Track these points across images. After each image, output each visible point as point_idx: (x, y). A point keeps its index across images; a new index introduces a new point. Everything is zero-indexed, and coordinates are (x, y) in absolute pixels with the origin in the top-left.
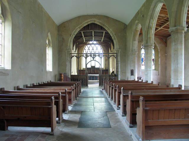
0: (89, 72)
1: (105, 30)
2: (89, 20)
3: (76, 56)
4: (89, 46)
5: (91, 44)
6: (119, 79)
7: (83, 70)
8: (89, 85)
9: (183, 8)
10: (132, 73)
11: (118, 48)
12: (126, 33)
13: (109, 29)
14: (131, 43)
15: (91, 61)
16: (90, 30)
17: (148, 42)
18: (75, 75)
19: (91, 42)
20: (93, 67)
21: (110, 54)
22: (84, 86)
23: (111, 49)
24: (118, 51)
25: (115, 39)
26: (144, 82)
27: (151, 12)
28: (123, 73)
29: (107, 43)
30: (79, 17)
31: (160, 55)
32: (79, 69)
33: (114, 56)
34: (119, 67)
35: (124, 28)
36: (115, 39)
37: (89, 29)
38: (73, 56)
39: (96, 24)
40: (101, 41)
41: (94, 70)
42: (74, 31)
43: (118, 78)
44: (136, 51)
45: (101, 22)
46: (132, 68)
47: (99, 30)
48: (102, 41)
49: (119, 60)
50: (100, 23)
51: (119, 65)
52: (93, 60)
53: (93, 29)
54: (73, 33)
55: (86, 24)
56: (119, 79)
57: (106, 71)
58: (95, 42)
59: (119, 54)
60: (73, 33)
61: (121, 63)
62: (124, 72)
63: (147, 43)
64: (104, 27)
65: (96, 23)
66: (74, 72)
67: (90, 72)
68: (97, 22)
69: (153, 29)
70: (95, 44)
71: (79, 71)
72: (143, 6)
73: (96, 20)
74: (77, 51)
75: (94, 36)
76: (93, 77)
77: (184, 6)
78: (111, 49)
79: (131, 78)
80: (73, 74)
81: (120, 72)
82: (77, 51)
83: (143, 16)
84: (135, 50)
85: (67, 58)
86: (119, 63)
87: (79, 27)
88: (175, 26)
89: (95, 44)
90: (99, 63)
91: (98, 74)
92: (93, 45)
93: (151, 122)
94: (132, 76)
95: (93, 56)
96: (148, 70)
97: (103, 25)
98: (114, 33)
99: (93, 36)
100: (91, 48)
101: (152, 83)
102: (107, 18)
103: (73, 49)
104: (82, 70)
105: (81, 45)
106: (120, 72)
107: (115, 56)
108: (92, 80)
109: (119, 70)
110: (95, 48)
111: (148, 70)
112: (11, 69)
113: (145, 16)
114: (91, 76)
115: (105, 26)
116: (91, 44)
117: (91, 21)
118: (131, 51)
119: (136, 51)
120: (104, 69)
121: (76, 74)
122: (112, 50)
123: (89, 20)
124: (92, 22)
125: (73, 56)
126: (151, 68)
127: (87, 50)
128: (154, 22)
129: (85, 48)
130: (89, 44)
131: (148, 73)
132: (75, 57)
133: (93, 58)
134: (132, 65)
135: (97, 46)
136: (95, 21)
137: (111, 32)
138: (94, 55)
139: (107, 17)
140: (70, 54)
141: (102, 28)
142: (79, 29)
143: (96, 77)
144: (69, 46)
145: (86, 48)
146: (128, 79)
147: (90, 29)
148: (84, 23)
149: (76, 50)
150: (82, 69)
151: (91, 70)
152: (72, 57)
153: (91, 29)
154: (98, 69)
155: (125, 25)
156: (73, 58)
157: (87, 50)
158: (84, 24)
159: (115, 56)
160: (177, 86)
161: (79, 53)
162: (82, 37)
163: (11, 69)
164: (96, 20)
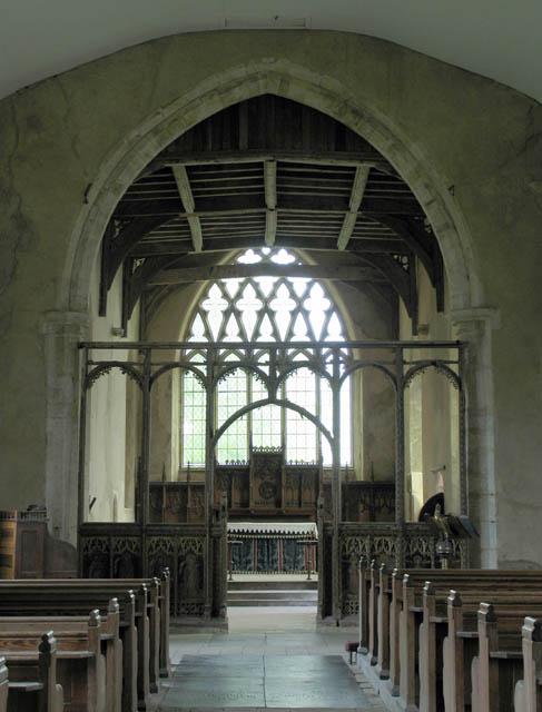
0: (236, 498)
1: (365, 150)
2: (240, 72)
3: (125, 367)
4: (232, 284)
6: (491, 563)
7: (187, 489)
8: (231, 612)
11: (477, 300)
13: (399, 145)
15: (247, 410)
18: (114, 529)
19: (249, 257)
21: (367, 541)
22: (194, 620)
23: (413, 313)
24: (479, 324)
30: (152, 42)
32: (153, 477)
34: (489, 462)
36: (450, 226)
38: (105, 367)
40: (332, 243)
41: (276, 489)
42: (119, 154)
45: (332, 84)
48: (342, 244)
49: (486, 398)
50: (329, 95)
51: (489, 441)
52: (272, 400)
54: (104, 175)
56: (491, 563)
57: (375, 492)
58: (284, 257)
59: (486, 356)
60: (104, 175)
65: (293, 93)
66: (111, 499)
67: (245, 503)
68: (306, 87)
70: (283, 272)
71: (151, 490)
73: (295, 70)
74: (132, 324)
75: (281, 202)
76: (267, 542)
78: (413, 313)
80: (99, 514)
81: (492, 500)
82: (132, 324)
85: (51, 380)
86: (488, 423)
87: (155, 131)
90: (315, 426)
91: (304, 518)
92: (266, 282)
97: (355, 112)
99: (271, 200)
100: (249, 305)
102: (384, 54)
103: (102, 311)
104: (173, 488)
106: (492, 500)
107: (455, 368)
109: (491, 484)
110: (283, 305)
114: (246, 539)
115: (371, 120)
116: (248, 272)
117: (253, 78)
120: (361, 477)
121: (125, 516)
122: (422, 320)
123: (240, 72)
125: (105, 367)
127: (215, 323)
129: (205, 305)
132: (116, 371)
133: (273, 383)
135: (300, 284)
136: (285, 79)
140: (81, 346)
141: (342, 138)
142: (154, 140)
143: (292, 541)
144: (73, 284)
147: (243, 143)
149: (125, 316)
150: (173, 476)
151: (245, 487)
152: (95, 375)
153: (253, 148)
154: (310, 476)
156: (101, 383)
157: (215, 323)
159: (455, 368)
161: (155, 337)
164: (295, 70)
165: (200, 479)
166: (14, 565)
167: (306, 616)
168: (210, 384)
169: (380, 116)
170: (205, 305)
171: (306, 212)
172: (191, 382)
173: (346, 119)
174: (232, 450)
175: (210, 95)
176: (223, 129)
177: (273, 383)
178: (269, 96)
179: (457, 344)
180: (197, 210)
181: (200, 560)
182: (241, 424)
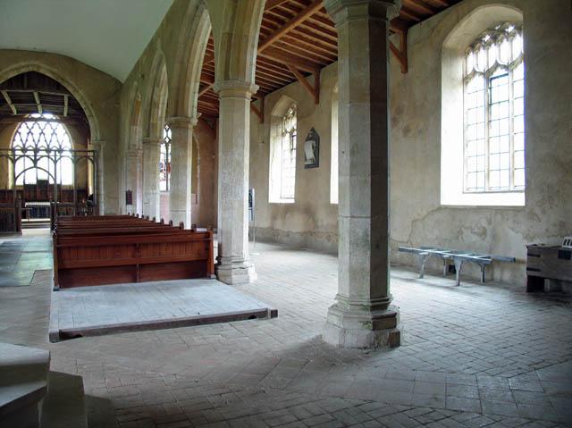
1: (68, 92)
2: (23, 64)
4: (30, 124)
5: (33, 119)
6: (102, 214)
8: (23, 230)
9: (187, 84)
10: (130, 199)
12: (118, 103)
13: (75, 90)
14: (127, 130)
15: (24, 171)
16: (27, 89)
17: (151, 135)
19: (35, 116)
20: (42, 184)
24: (100, 146)
25: (91, 116)
26: (102, 218)
27: (155, 72)
28: (110, 198)
29: (77, 122)
31: (199, 158)
33: (48, 157)
34: (102, 186)
35: (112, 91)
36: (91, 116)
37: (22, 85)
39: (44, 76)
40: (62, 114)
41: (46, 192)
43: (97, 207)
44: (137, 147)
45: (55, 70)
46: (129, 188)
47: (50, 90)
48: (65, 114)
49: (101, 166)
50: (53, 73)
51: (102, 179)
53: (34, 88)
55: (15, 74)
56: (102, 214)
58: (48, 116)
59: (102, 155)
61: (106, 174)
62: (112, 196)
63: (148, 136)
64: (65, 85)
65: (42, 71)
66: (10, 187)
67: (36, 196)
68: (45, 70)
69: (160, 106)
70: (49, 121)
72: (144, 54)
73: (42, 65)
77: (189, 81)
79: (126, 210)
83: (143, 76)
84: (134, 145)
86: (102, 174)
88: (176, 116)
89: (49, 121)
91: (48, 201)
92: (42, 124)
93: (68, 264)
94: (129, 206)
95: (53, 158)
96: (149, 194)
97: (62, 79)
98: (89, 103)
100: (36, 131)
101: (180, 228)
102: (72, 63)
105: (6, 121)
108: (40, 217)
110: (48, 131)
111: (149, 194)
112: (524, 205)
113: (146, 76)
115: (68, 82)
116: (36, 120)
117: (28, 66)
118: (126, 147)
119: (137, 147)
121: (337, 202)
124: (31, 69)
126: (155, 188)
127: (24, 136)
128: (162, 93)
129: (20, 130)
130: (33, 119)
131: (149, 200)
133: (35, 161)
134: (129, 180)
135: (54, 124)
136: (39, 67)
137: (82, 98)
138: (54, 153)
139: (72, 61)
141: (58, 87)
143: (43, 208)
145: (23, 128)
146: (121, 212)
147: (25, 86)
148: (8, 69)
151: (35, 191)
153: (28, 87)
155: (117, 82)
157: (24, 136)
158: (7, 73)
160: (178, 225)
162: (6, 102)
163: (524, 205)
164: (42, 65)
165: (22, 188)
166: (190, 133)
167: (155, 212)
168: (14, 162)
169: (71, 82)
170: (20, 130)
171: (52, 104)
172: (10, 162)
173: (60, 81)
174: (19, 182)
175: (13, 70)
176: (18, 81)
177: (35, 161)
178: (34, 72)
179: (92, 151)
180: (13, 103)
181: (12, 215)
182: (23, 174)
